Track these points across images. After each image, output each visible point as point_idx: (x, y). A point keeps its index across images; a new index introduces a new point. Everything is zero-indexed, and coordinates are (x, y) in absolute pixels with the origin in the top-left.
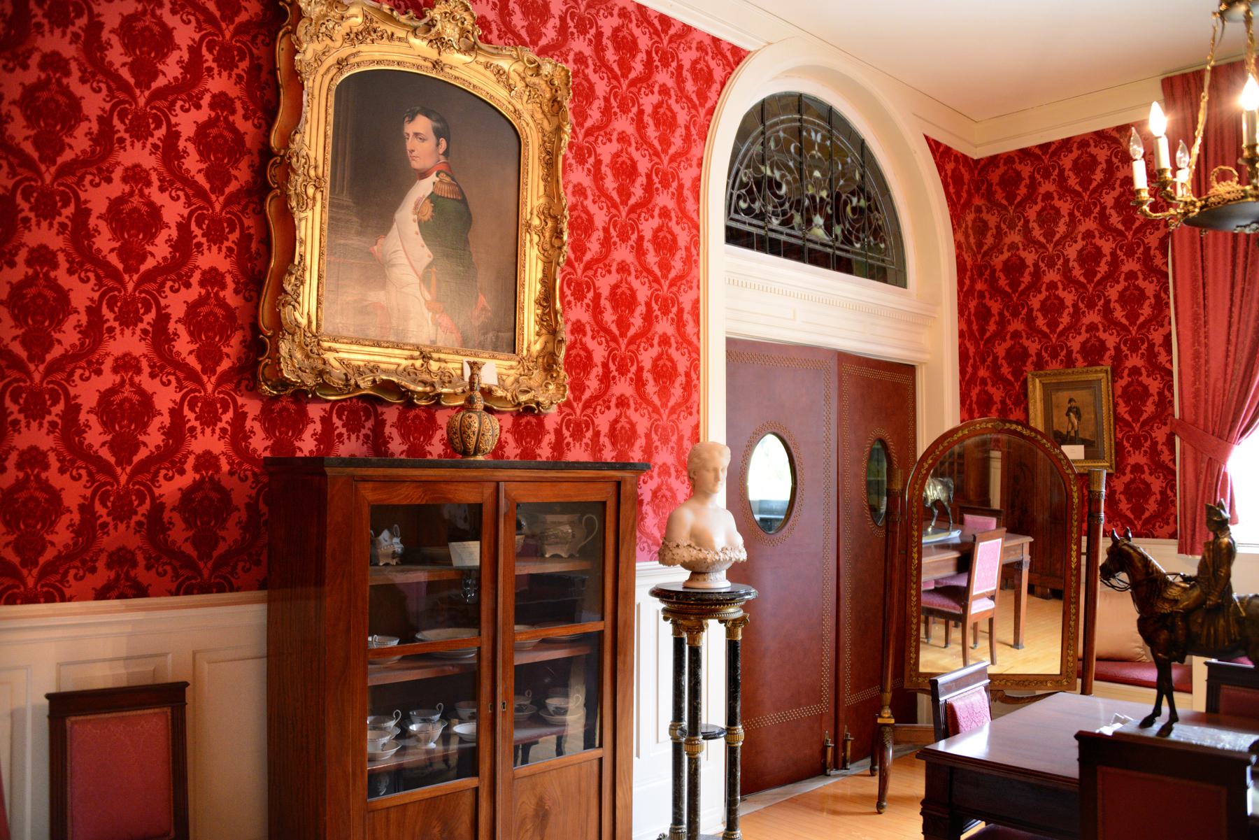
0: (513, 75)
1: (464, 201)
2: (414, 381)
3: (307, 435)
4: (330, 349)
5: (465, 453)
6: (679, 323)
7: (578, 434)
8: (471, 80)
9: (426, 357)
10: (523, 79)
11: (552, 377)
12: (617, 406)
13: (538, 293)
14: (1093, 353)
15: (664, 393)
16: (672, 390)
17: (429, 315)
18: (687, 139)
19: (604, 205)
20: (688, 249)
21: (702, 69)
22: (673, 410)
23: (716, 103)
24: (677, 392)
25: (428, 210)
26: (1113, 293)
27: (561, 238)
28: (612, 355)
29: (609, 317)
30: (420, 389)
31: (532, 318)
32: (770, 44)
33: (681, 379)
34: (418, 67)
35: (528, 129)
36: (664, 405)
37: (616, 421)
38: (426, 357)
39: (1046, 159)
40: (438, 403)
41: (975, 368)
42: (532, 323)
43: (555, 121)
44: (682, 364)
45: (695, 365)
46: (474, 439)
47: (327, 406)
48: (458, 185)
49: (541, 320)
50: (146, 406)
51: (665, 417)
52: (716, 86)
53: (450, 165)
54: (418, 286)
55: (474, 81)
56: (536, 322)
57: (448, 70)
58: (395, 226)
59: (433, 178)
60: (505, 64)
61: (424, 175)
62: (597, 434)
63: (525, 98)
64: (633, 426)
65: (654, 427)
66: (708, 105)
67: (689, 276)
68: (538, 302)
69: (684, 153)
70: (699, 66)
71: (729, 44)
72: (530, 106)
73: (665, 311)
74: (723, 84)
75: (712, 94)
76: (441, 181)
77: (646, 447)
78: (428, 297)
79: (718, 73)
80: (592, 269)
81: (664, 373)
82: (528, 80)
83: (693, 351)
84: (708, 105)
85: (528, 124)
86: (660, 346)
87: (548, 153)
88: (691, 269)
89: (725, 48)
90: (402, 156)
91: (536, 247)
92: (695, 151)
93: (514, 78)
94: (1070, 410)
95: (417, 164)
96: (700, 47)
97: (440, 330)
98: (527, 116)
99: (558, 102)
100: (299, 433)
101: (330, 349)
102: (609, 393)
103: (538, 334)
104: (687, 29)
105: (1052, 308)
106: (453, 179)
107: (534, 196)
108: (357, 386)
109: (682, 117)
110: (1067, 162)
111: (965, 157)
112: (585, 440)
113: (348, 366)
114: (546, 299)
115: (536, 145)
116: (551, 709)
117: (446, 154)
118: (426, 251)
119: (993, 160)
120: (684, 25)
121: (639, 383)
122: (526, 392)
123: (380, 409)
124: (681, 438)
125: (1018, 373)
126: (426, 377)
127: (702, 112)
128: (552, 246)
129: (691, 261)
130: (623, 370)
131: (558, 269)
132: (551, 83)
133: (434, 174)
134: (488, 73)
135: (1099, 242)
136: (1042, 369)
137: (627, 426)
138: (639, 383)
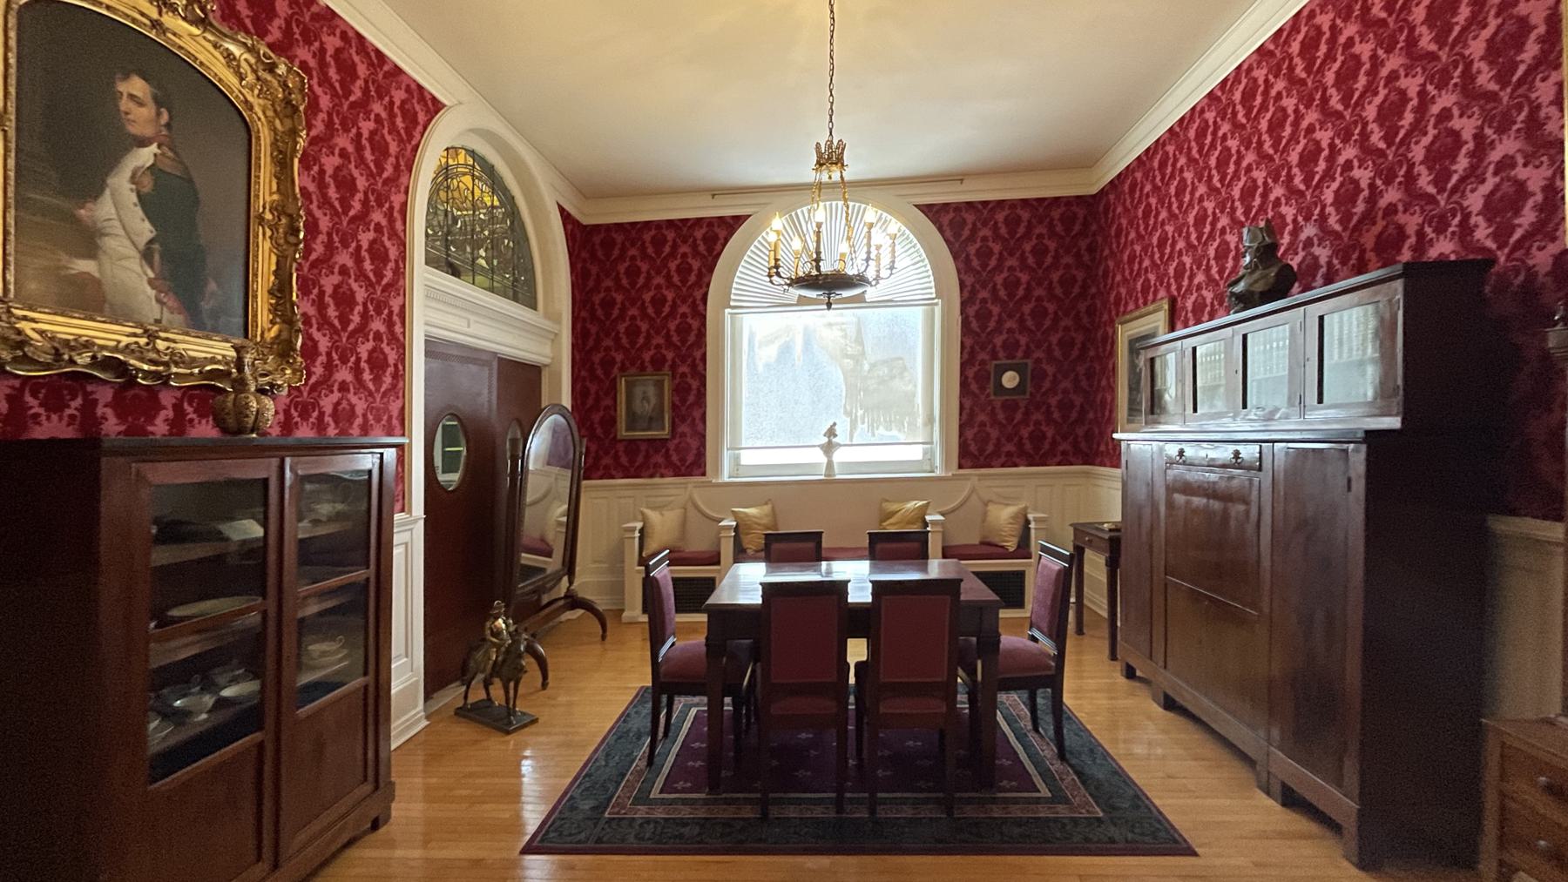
0: (244, 64)
1: (190, 181)
2: (142, 360)
3: (159, 421)
4: (25, 318)
5: (241, 430)
6: (390, 323)
7: (304, 415)
8: (197, 55)
9: (152, 337)
10: (255, 71)
11: (288, 362)
12: (339, 390)
13: (271, 284)
14: (658, 363)
15: (377, 380)
16: (384, 379)
17: (152, 293)
18: (397, 167)
19: (328, 212)
20: (396, 262)
21: (408, 110)
22: (384, 394)
23: (419, 142)
24: (388, 380)
25: (148, 184)
26: (672, 326)
27: (298, 236)
28: (335, 346)
29: (332, 312)
30: (146, 367)
31: (266, 307)
32: (461, 103)
33: (391, 370)
34: (134, 20)
35: (259, 123)
36: (378, 390)
37: (338, 404)
38: (152, 337)
39: (633, 232)
40: (166, 384)
41: (579, 371)
42: (266, 312)
43: (288, 122)
44: (392, 357)
45: (402, 358)
46: (253, 417)
47: (17, 383)
48: (181, 163)
49: (274, 310)
50: (614, 302)
51: (378, 400)
52: (420, 128)
53: (170, 138)
54: (138, 260)
55: (201, 57)
56: (269, 310)
57: (169, 35)
58: (107, 192)
59: (154, 148)
60: (235, 50)
61: (143, 142)
62: (322, 414)
63: (256, 92)
64: (352, 407)
65: (370, 408)
66: (414, 143)
67: (397, 284)
68: (270, 292)
69: (393, 181)
70: (407, 107)
71: (431, 94)
72: (261, 101)
73: (379, 312)
74: (425, 128)
75: (417, 134)
76: (163, 154)
77: (284, 423)
78: (151, 275)
79: (421, 117)
80: (316, 268)
81: (377, 363)
82: (260, 74)
83: (401, 347)
84: (414, 143)
85: (259, 119)
86: (374, 341)
87: (281, 152)
88: (398, 279)
89: (428, 97)
90: (116, 120)
91: (269, 240)
92: (403, 180)
93: (245, 67)
94: (643, 399)
95: (134, 129)
96: (408, 90)
97: (165, 309)
98: (257, 109)
99: (293, 106)
100: (151, 419)
101: (25, 318)
102: (332, 379)
103: (273, 322)
104: (398, 71)
105: (633, 332)
106: (175, 153)
107: (266, 190)
108: (72, 362)
109: (393, 148)
110: (647, 237)
111: (578, 221)
112: (311, 420)
113: (52, 339)
114: (280, 290)
115: (268, 142)
116: (315, 655)
117: (168, 126)
118: (147, 225)
119: (597, 228)
120: (396, 66)
121: (357, 371)
122: (266, 375)
123: (89, 388)
124: (390, 417)
125: (607, 373)
126: (153, 356)
127: (409, 148)
128: (287, 242)
129: (399, 273)
130: (344, 360)
131: (295, 265)
132: (285, 85)
133: (155, 145)
134: (217, 54)
135: (666, 292)
136: (624, 371)
137: (348, 407)
138: (357, 371)
